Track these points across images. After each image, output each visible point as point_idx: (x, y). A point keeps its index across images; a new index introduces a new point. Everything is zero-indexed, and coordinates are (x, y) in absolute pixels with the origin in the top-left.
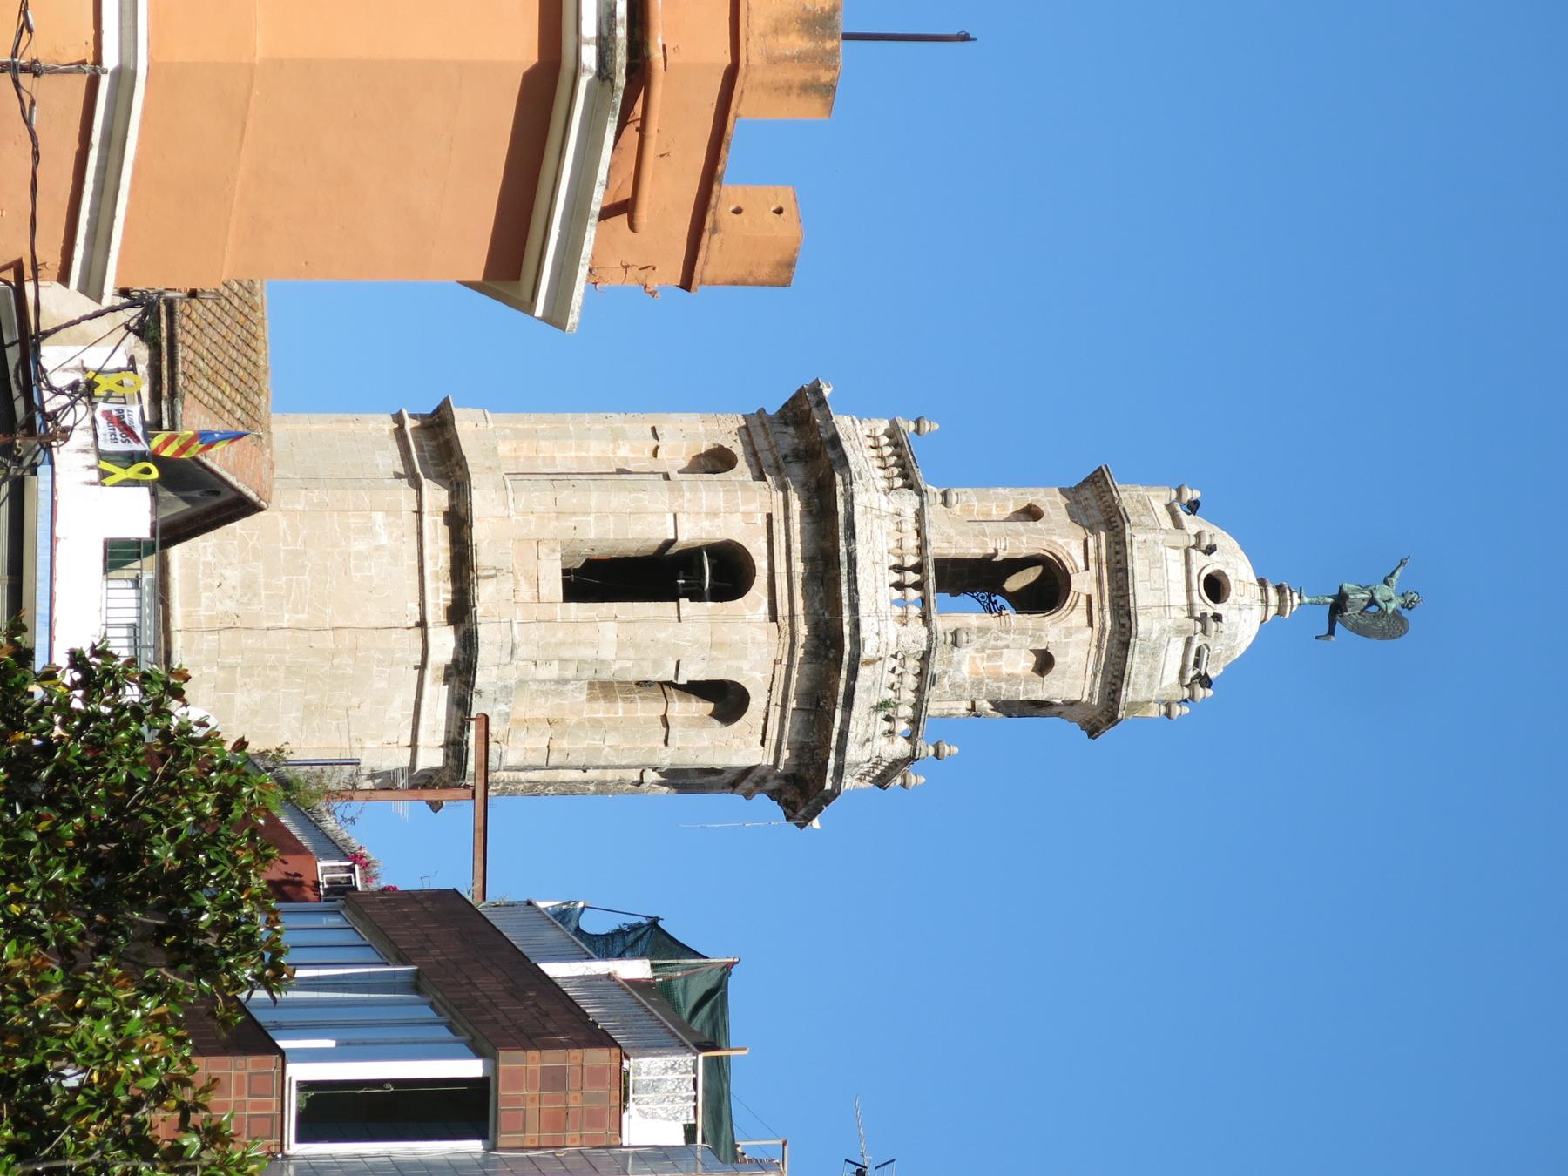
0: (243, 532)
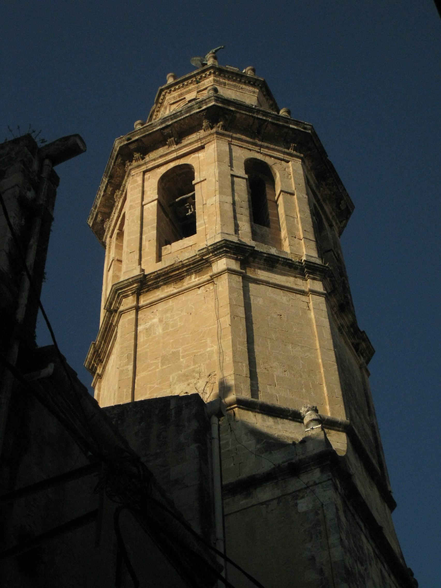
0: (148, 393)
